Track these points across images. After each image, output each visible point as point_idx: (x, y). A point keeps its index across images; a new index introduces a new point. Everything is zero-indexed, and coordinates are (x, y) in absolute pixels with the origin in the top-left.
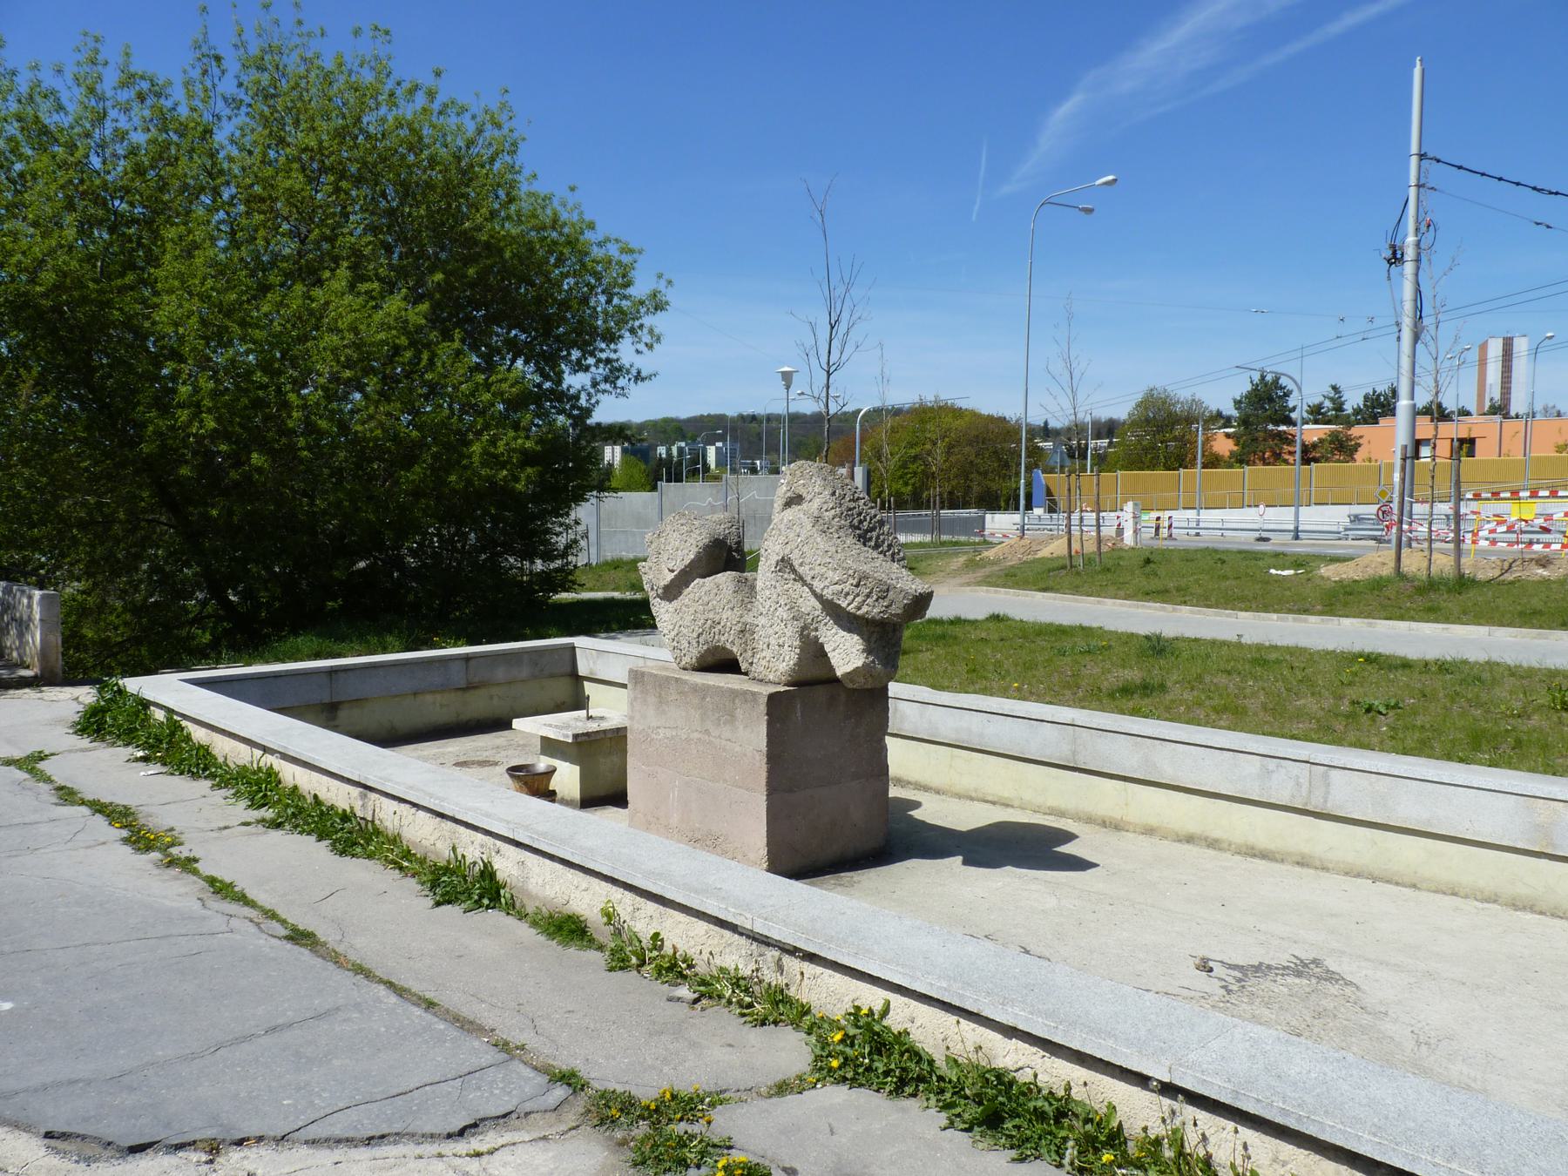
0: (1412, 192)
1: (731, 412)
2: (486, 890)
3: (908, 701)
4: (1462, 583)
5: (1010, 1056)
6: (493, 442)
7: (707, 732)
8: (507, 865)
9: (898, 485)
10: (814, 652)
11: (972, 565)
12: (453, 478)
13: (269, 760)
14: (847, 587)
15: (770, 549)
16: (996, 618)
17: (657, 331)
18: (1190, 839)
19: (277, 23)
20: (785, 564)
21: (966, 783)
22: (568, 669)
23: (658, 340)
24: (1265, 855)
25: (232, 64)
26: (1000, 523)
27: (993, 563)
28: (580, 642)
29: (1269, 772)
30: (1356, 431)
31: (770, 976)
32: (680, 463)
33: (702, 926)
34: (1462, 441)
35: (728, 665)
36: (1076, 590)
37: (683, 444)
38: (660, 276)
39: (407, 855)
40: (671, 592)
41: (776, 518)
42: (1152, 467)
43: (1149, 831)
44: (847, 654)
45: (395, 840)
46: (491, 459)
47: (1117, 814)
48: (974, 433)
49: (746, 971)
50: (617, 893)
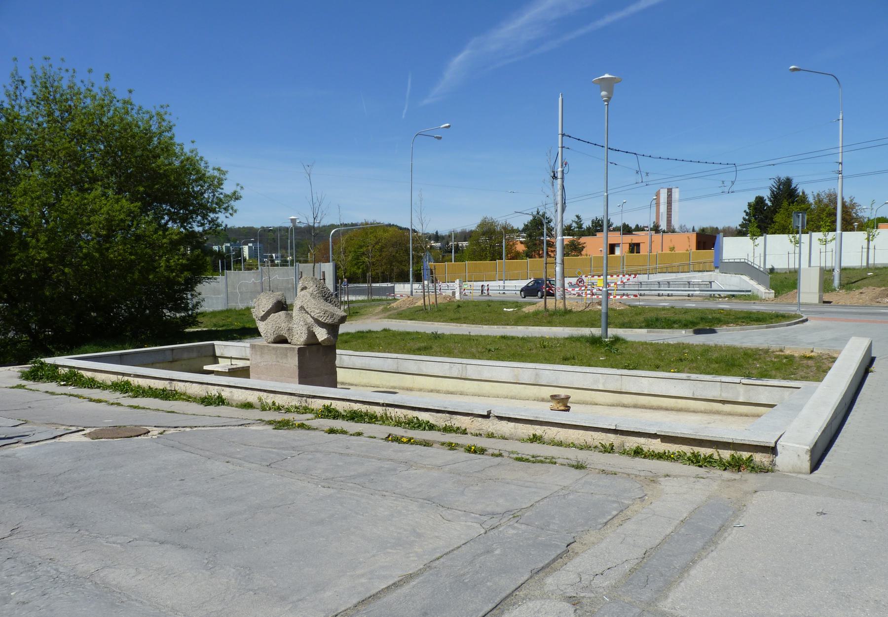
0: (560, 149)
1: (257, 225)
2: (220, 401)
3: (343, 356)
4: (567, 312)
5: (356, 407)
6: (168, 260)
8: (226, 393)
9: (354, 269)
10: (312, 335)
11: (385, 310)
12: (151, 277)
13: (126, 378)
15: (297, 304)
16: (385, 330)
17: (235, 208)
18: (432, 391)
19: (51, 66)
20: (302, 308)
21: (365, 381)
22: (212, 353)
23: (236, 211)
24: (452, 393)
25: (28, 82)
26: (402, 289)
27: (395, 309)
28: (215, 342)
30: (583, 240)
31: (304, 404)
32: (229, 257)
33: (286, 397)
34: (634, 244)
35: (284, 341)
36: (424, 319)
37: (229, 245)
38: (238, 185)
39: (190, 397)
40: (264, 318)
41: (298, 294)
42: (485, 259)
43: (420, 390)
44: (322, 335)
45: (184, 394)
46: (169, 268)
48: (394, 240)
49: (298, 405)
50: (261, 394)
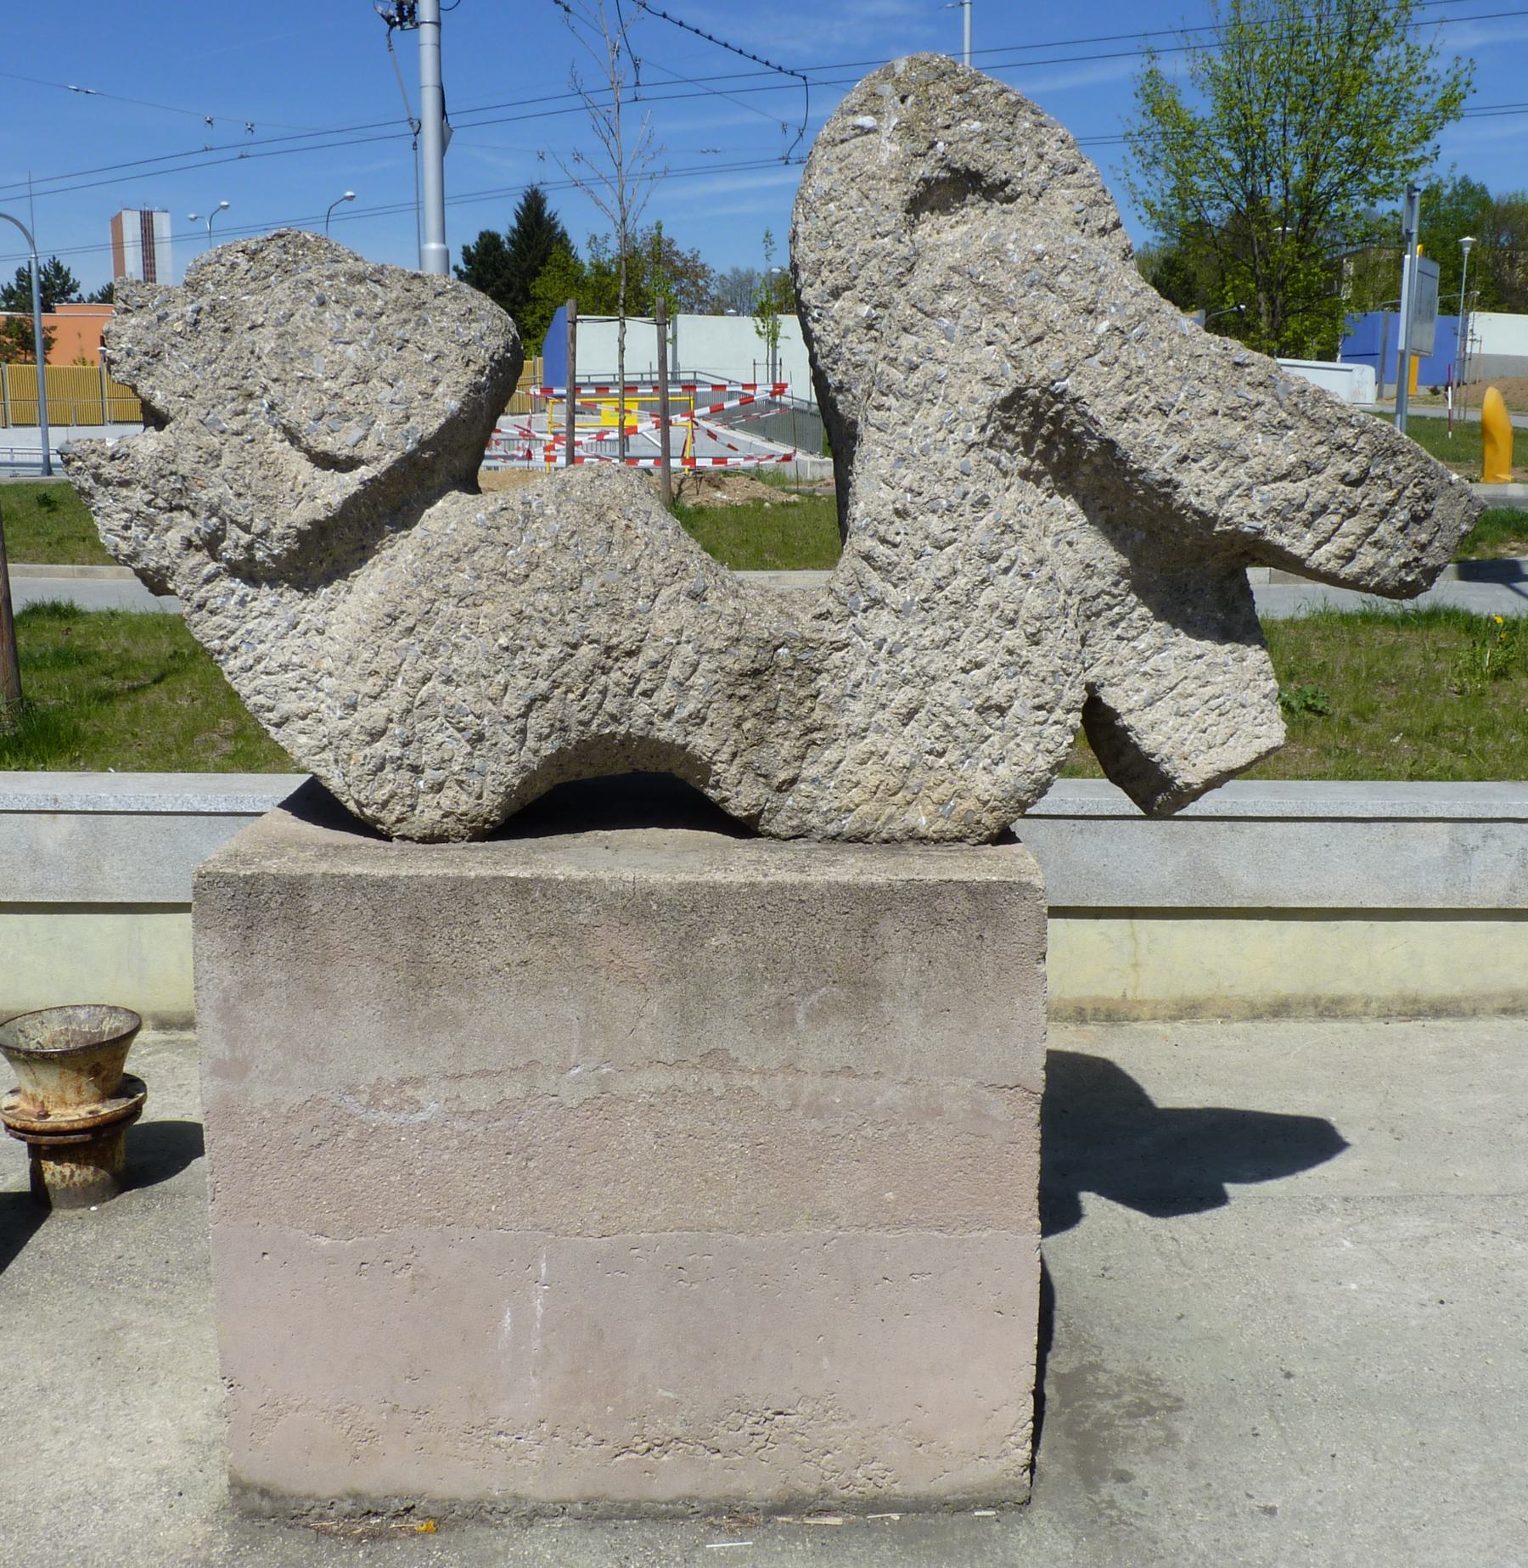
7: (717, 1059)
14: (1321, 488)
18: (1280, 1009)
24: (1439, 1009)
29: (1468, 851)
43: (1189, 1010)
47: (1111, 989)
